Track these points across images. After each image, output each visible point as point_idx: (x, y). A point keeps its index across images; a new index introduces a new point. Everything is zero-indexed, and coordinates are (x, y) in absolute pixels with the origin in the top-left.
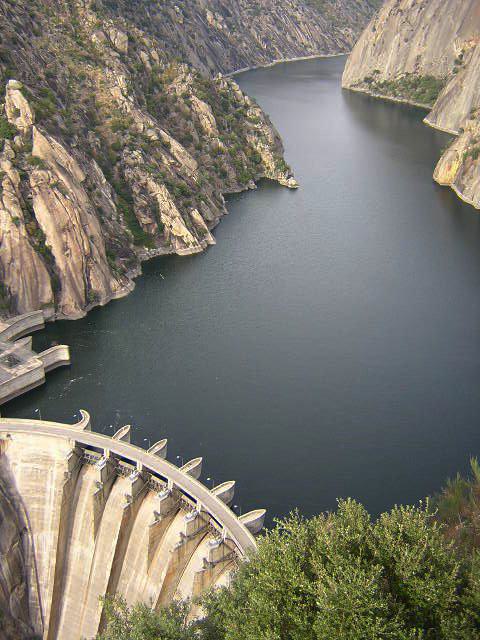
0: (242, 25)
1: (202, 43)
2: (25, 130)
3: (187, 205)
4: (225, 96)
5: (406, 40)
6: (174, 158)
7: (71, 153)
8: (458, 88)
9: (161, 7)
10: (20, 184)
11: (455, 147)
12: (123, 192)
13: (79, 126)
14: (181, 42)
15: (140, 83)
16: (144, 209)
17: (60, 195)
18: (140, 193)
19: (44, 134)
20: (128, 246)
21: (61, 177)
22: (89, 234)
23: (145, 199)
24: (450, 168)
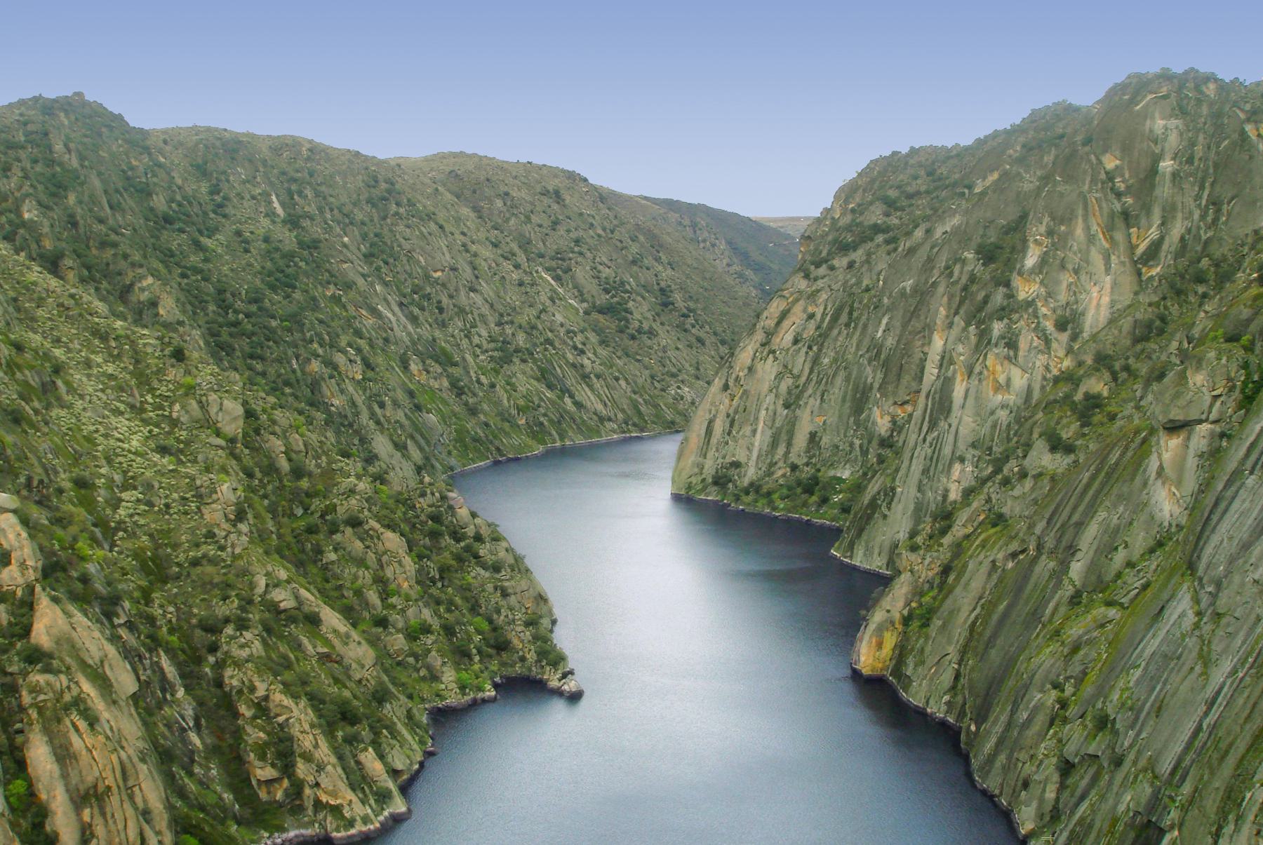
0: (478, 381)
1: (400, 415)
2: (19, 593)
3: (351, 740)
4: (436, 518)
6: (327, 642)
7: (114, 639)
8: (889, 493)
9: (320, 351)
11: (886, 603)
12: (220, 708)
13: (133, 582)
14: (357, 414)
15: (265, 496)
17: (82, 725)
18: (255, 717)
19: (55, 600)
21: (87, 687)
22: (141, 805)
23: (262, 729)
24: (880, 645)
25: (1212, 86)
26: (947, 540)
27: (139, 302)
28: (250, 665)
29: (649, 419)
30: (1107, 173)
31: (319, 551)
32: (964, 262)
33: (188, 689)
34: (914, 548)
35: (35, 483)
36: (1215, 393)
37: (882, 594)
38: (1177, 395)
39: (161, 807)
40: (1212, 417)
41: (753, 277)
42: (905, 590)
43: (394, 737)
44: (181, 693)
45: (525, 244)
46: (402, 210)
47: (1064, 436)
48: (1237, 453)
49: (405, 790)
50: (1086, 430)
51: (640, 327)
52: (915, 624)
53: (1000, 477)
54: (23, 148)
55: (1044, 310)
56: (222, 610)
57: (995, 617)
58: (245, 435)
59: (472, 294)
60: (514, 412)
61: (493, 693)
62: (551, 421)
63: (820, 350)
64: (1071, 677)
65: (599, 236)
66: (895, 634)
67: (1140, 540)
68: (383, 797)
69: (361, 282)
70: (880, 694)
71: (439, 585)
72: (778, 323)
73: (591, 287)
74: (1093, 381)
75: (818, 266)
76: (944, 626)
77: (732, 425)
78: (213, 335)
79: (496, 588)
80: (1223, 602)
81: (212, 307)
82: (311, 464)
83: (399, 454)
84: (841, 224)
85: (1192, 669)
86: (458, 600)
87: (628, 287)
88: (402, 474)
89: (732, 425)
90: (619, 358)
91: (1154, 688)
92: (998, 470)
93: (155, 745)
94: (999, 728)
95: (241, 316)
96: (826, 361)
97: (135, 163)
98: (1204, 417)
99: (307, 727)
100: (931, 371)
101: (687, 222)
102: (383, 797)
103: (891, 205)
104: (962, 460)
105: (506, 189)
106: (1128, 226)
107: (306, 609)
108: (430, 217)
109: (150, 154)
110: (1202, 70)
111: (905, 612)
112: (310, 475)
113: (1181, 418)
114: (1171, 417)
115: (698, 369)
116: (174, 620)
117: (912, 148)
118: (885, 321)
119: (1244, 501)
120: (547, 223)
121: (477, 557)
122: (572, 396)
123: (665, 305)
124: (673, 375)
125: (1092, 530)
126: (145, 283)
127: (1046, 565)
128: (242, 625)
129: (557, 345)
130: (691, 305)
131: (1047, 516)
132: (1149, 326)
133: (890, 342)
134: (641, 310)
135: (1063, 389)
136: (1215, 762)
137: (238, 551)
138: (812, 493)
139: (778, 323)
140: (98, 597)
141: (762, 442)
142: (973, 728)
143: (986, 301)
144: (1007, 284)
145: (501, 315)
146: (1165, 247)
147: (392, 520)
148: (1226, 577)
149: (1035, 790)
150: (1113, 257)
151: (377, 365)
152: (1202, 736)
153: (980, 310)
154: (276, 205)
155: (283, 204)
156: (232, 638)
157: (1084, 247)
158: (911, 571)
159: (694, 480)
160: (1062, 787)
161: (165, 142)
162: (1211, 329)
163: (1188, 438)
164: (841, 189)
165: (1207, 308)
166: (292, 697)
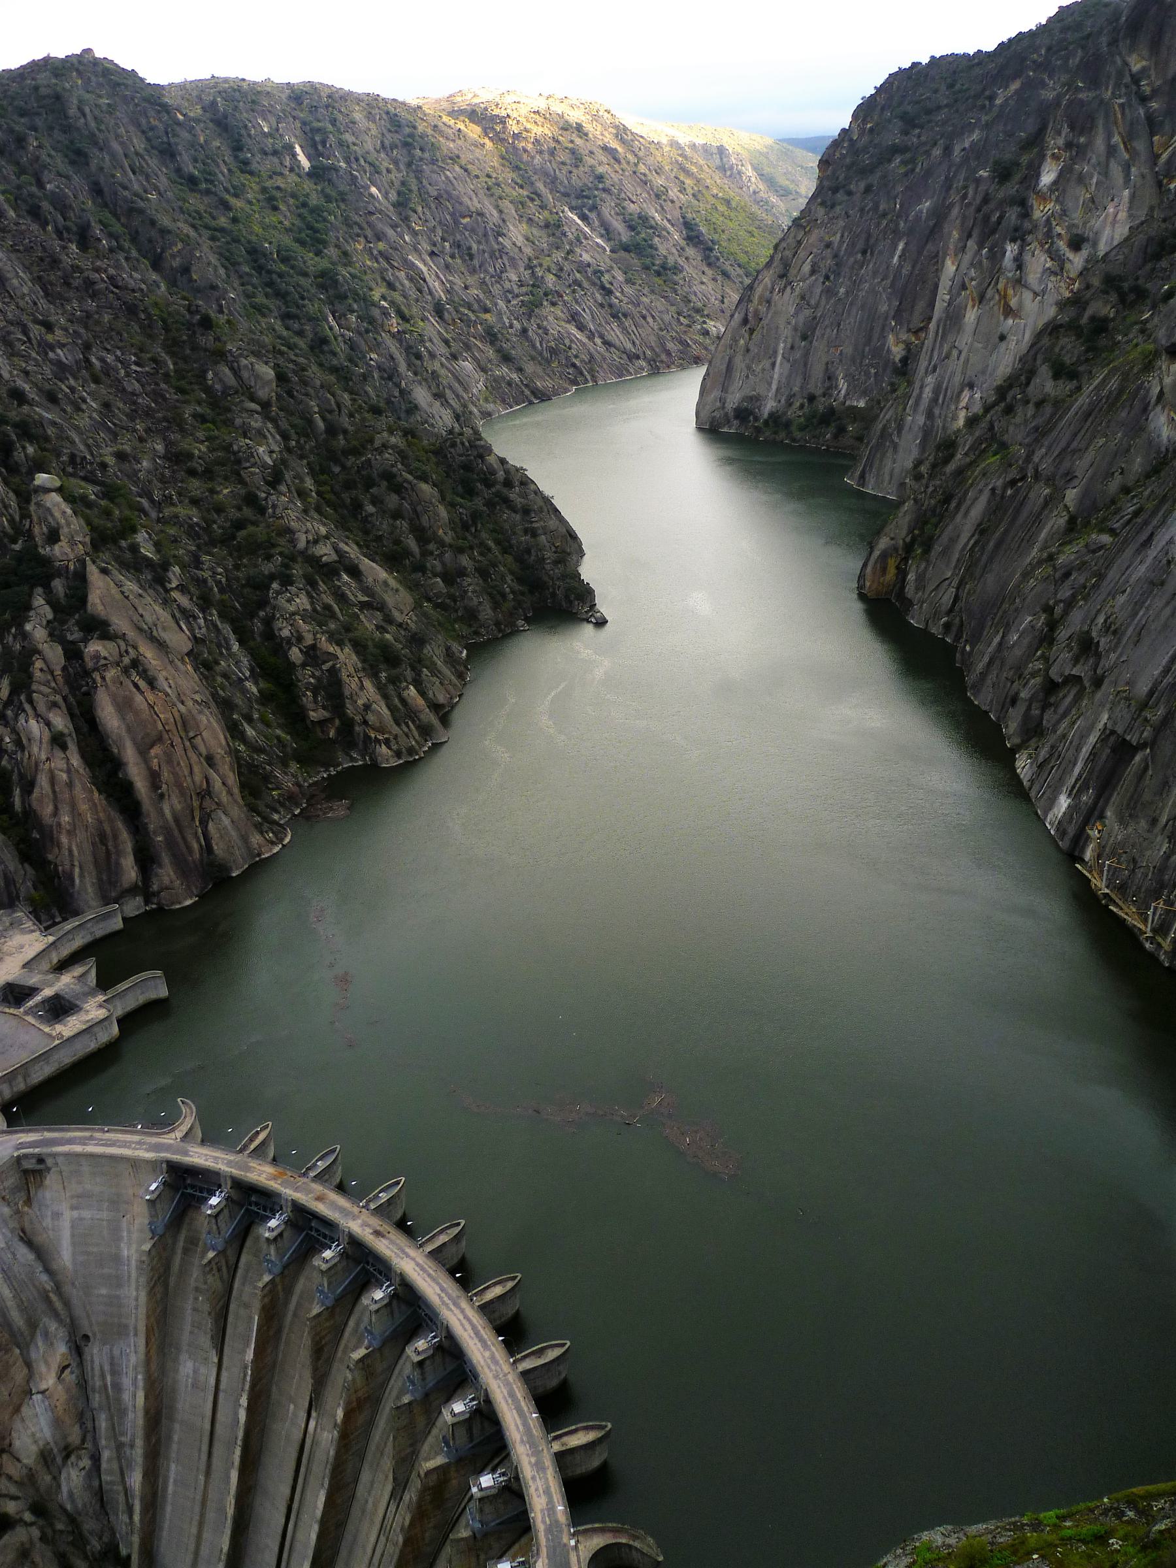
3: (394, 681)
4: (467, 467)
5: (804, 337)
9: (355, 306)
10: (64, 669)
17: (142, 684)
18: (304, 665)
19: (104, 571)
24: (884, 570)
26: (950, 468)
30: (1132, 76)
31: (357, 506)
33: (241, 642)
35: (78, 460)
42: (907, 518)
43: (433, 674)
44: (236, 647)
45: (552, 182)
50: (1090, 355)
53: (1003, 405)
54: (38, 114)
55: (1058, 229)
56: (268, 568)
58: (279, 397)
59: (500, 239)
60: (546, 354)
62: (582, 361)
64: (1061, 601)
67: (1138, 464)
69: (390, 232)
73: (618, 225)
74: (1100, 303)
79: (526, 531)
82: (345, 421)
84: (860, 145)
86: (490, 543)
87: (653, 223)
91: (1137, 614)
93: (214, 696)
97: (154, 122)
100: (943, 296)
104: (971, 386)
106: (1152, 134)
109: (168, 113)
111: (908, 539)
112: (345, 432)
115: (723, 302)
116: (224, 580)
118: (901, 246)
121: (506, 501)
124: (698, 311)
128: (287, 581)
138: (828, 424)
140: (149, 562)
141: (781, 374)
142: (968, 648)
143: (999, 222)
147: (424, 472)
150: (1133, 169)
151: (412, 317)
153: (993, 232)
155: (309, 158)
156: (278, 593)
157: (1103, 159)
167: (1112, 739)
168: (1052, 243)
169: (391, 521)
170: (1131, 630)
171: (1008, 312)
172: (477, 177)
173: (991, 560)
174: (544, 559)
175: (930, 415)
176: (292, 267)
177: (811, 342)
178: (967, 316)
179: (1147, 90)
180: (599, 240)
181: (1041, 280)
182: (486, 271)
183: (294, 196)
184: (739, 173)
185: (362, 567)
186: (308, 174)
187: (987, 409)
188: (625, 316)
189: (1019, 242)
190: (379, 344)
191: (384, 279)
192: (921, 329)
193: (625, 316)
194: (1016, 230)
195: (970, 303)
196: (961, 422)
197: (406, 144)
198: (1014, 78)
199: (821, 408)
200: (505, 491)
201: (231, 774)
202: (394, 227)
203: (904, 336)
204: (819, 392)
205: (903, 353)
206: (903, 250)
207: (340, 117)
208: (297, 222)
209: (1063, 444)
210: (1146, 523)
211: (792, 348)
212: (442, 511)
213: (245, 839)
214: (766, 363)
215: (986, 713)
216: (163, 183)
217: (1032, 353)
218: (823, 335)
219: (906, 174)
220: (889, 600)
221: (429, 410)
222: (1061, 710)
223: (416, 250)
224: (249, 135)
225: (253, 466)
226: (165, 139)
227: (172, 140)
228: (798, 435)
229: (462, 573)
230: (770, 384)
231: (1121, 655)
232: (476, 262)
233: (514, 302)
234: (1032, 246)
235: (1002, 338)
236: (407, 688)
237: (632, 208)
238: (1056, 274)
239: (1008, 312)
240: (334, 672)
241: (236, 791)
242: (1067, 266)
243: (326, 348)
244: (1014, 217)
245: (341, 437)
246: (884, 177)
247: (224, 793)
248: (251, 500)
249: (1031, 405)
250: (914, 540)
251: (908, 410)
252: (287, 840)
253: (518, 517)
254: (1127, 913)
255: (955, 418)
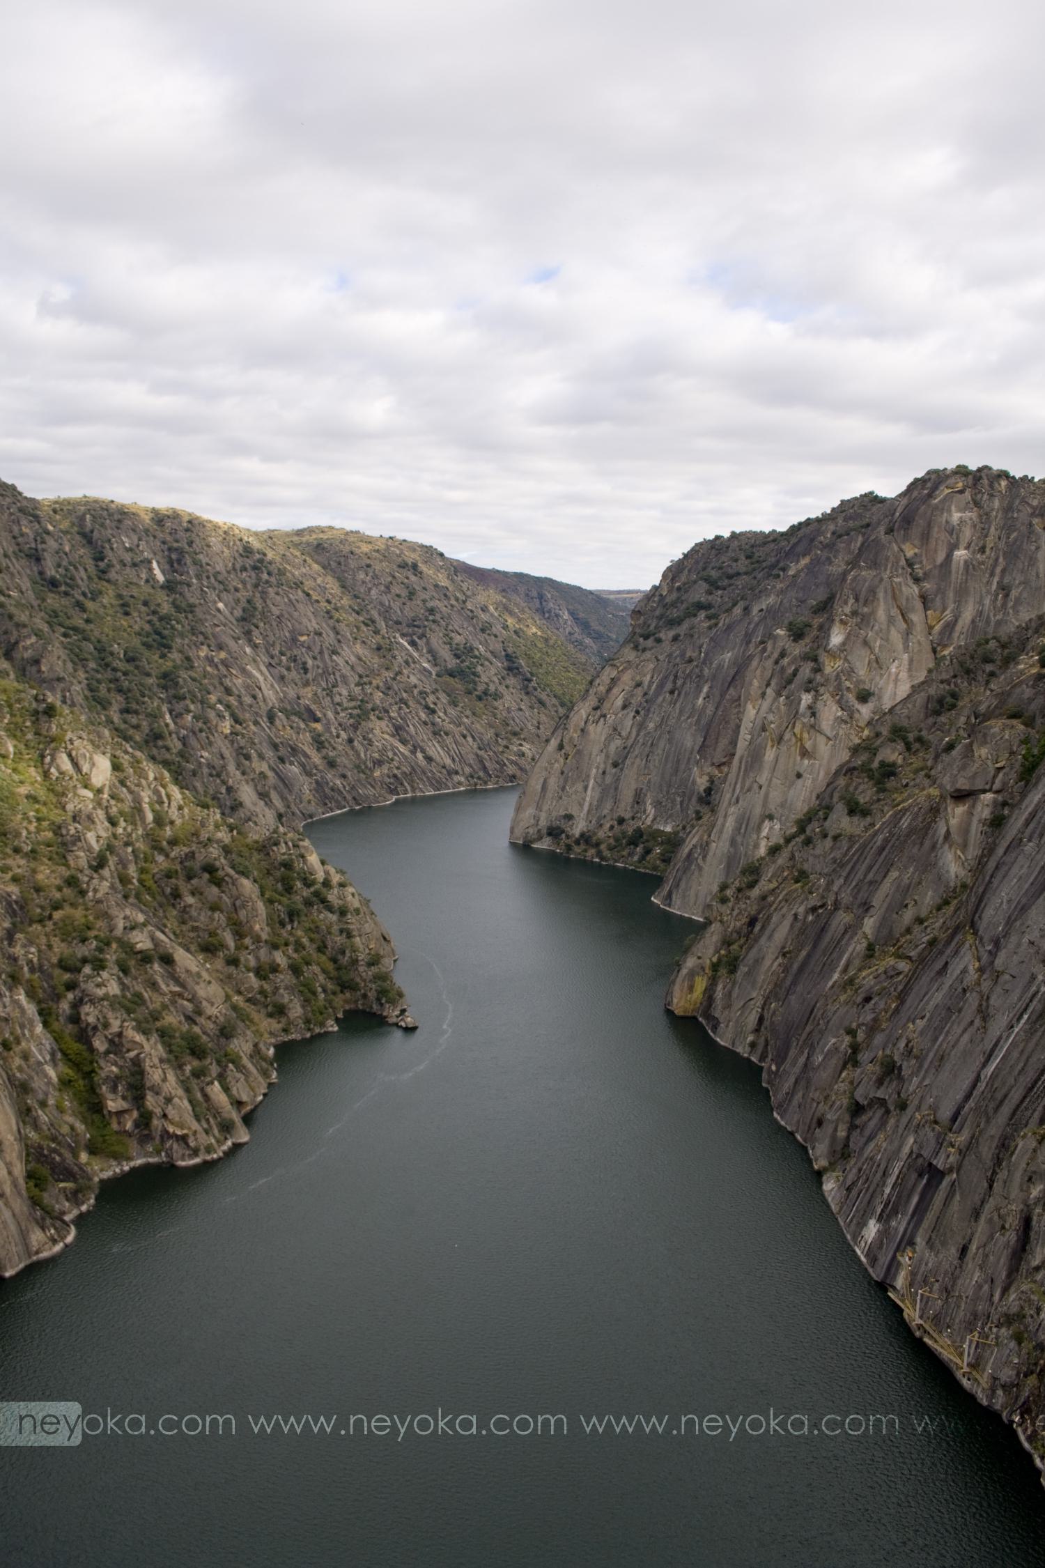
1: (264, 767)
4: (287, 865)
5: (615, 765)
8: (705, 847)
9: (192, 707)
16: (114, 1083)
18: (108, 1052)
20: (76, 1155)
23: (115, 1064)
24: (691, 989)
25: (1004, 483)
26: (756, 892)
27: (23, 659)
28: (105, 1003)
29: (490, 779)
30: (907, 560)
31: (176, 895)
32: (775, 638)
33: (46, 1024)
34: (724, 900)
36: (998, 765)
37: (694, 941)
38: (963, 768)
39: (12, 1139)
40: (995, 787)
41: (592, 644)
42: (715, 938)
44: (39, 1028)
45: (386, 612)
46: (273, 580)
47: (862, 801)
48: (1016, 822)
49: (248, 1120)
50: (882, 796)
51: (487, 690)
52: (723, 971)
53: (803, 837)
55: (848, 684)
56: (83, 951)
57: (796, 966)
60: (370, 764)
61: (336, 1029)
63: (646, 716)
65: (452, 606)
66: (706, 978)
67: (929, 898)
68: (227, 1128)
69: (232, 643)
70: (691, 1030)
71: (289, 927)
72: (609, 690)
73: (445, 653)
74: (889, 751)
75: (646, 637)
76: (749, 973)
77: (566, 781)
78: (91, 690)
79: (341, 931)
80: (999, 962)
81: (92, 665)
83: (262, 803)
84: (668, 600)
85: (972, 1022)
86: (305, 940)
87: (477, 653)
88: (264, 821)
89: (566, 781)
90: (467, 717)
91: (937, 1039)
92: (802, 830)
94: (797, 1069)
95: (119, 674)
96: (651, 725)
98: (987, 787)
99: (156, 1061)
100: (744, 736)
101: (534, 594)
102: (227, 1128)
103: (713, 585)
104: (771, 817)
105: (368, 562)
107: (161, 950)
108: (298, 585)
109: (39, 523)
110: (995, 468)
111: (715, 959)
112: (172, 823)
113: (967, 787)
114: (958, 786)
116: (35, 960)
117: (733, 533)
118: (705, 689)
119: (1022, 867)
120: (404, 593)
121: (324, 901)
122: (423, 751)
123: (509, 669)
124: (515, 734)
125: (886, 887)
126: (28, 642)
127: (843, 918)
128: (99, 965)
129: (410, 703)
130: (534, 670)
131: (844, 874)
132: (941, 701)
133: (709, 711)
134: (490, 674)
135: (864, 757)
136: (991, 1111)
137: (99, 895)
138: (637, 846)
139: (609, 690)
142: (774, 1068)
143: (795, 674)
144: (815, 659)
145: (361, 677)
146: (958, 628)
148: (1004, 937)
149: (828, 1129)
152: (981, 1086)
153: (790, 682)
154: (157, 572)
155: (163, 572)
156: (89, 977)
157: (884, 627)
158: (721, 921)
159: (531, 831)
160: (852, 1127)
161: (55, 511)
162: (996, 707)
163: (973, 806)
164: (669, 569)
165: (992, 686)
166: (144, 1033)
167: (920, 1161)
168: (842, 696)
169: (209, 913)
170: (931, 1055)
171: (804, 753)
172: (317, 601)
173: (794, 983)
174: (357, 961)
175: (733, 842)
176: (137, 667)
177: (622, 770)
178: (767, 754)
179: (920, 573)
180: (425, 665)
181: (833, 728)
182: (319, 684)
183: (145, 604)
184: (557, 616)
185: (176, 957)
186: (162, 587)
187: (788, 840)
188: (447, 734)
189: (813, 693)
190: (211, 744)
191: (221, 684)
192: (724, 764)
193: (447, 734)
194: (810, 682)
195: (770, 743)
196: (762, 851)
197: (255, 568)
198: (804, 555)
199: (630, 831)
200: (324, 890)
201: (19, 1165)
202: (236, 639)
203: (708, 769)
204: (627, 816)
205: (708, 784)
206: (708, 693)
207: (197, 540)
208: (147, 627)
209: (860, 875)
210: (941, 953)
211: (604, 773)
212: (260, 906)
213: (24, 1236)
214: (580, 786)
215: (792, 1134)
216: (26, 584)
217: (830, 789)
218: (633, 763)
219: (710, 628)
220: (695, 1018)
221: (253, 808)
222: (867, 1132)
223: (255, 661)
224: (112, 549)
225: (79, 849)
226: (33, 545)
227: (40, 547)
228: (607, 853)
229: (275, 969)
230: (581, 805)
231: (924, 1079)
232: (309, 676)
233: (343, 714)
234: (825, 697)
235: (799, 776)
236: (212, 1083)
237: (458, 639)
238: (846, 722)
239: (804, 753)
240: (137, 1062)
241: (21, 1181)
242: (856, 715)
243: (160, 743)
244: (807, 671)
245: (168, 828)
246: (692, 628)
247: (9, 1183)
248: (72, 882)
249: (829, 839)
250: (719, 960)
251: (712, 837)
252: (70, 1239)
253: (334, 918)
254: (941, 1346)
255: (756, 846)
